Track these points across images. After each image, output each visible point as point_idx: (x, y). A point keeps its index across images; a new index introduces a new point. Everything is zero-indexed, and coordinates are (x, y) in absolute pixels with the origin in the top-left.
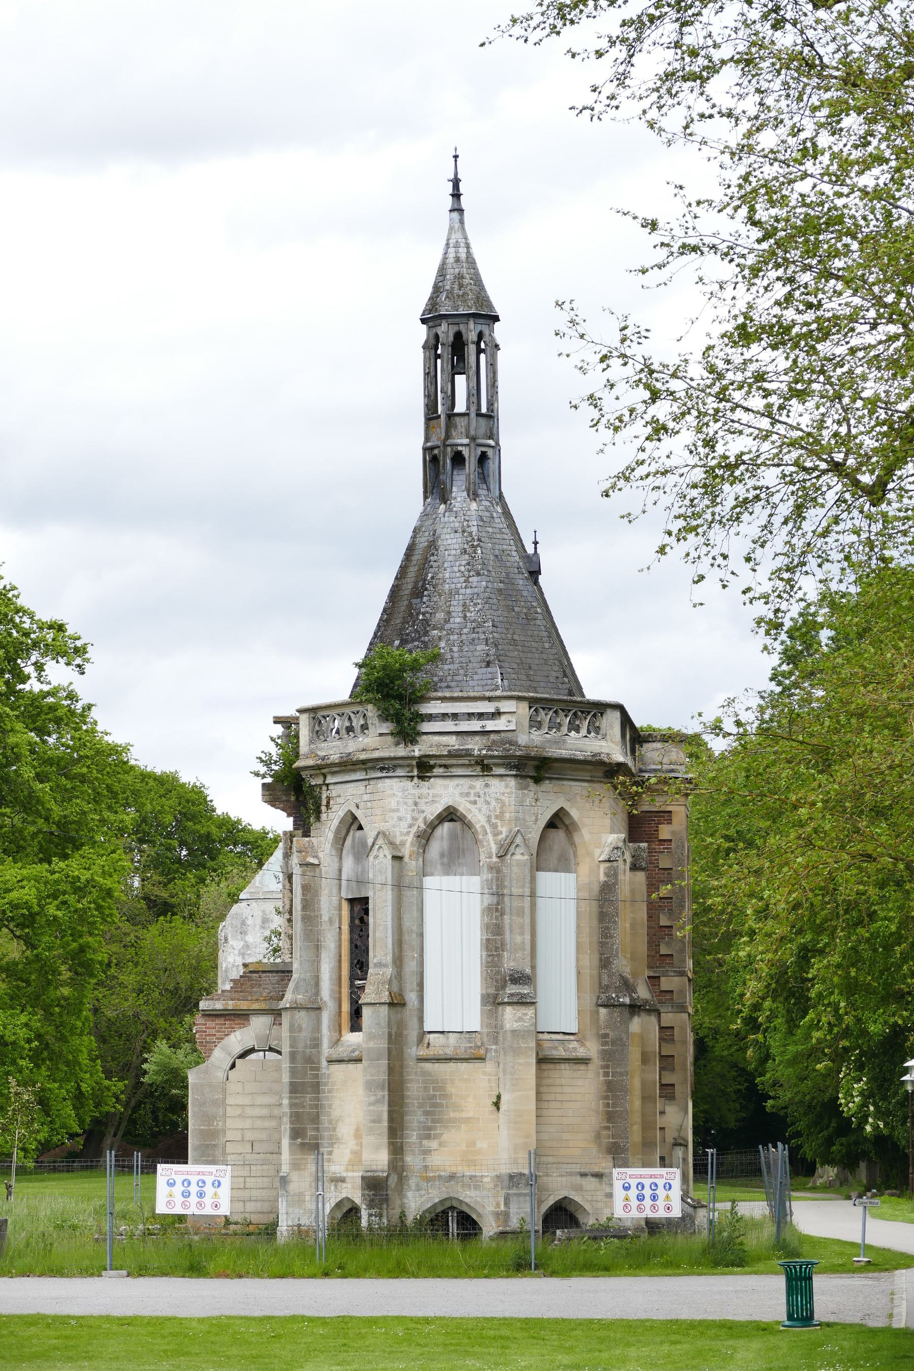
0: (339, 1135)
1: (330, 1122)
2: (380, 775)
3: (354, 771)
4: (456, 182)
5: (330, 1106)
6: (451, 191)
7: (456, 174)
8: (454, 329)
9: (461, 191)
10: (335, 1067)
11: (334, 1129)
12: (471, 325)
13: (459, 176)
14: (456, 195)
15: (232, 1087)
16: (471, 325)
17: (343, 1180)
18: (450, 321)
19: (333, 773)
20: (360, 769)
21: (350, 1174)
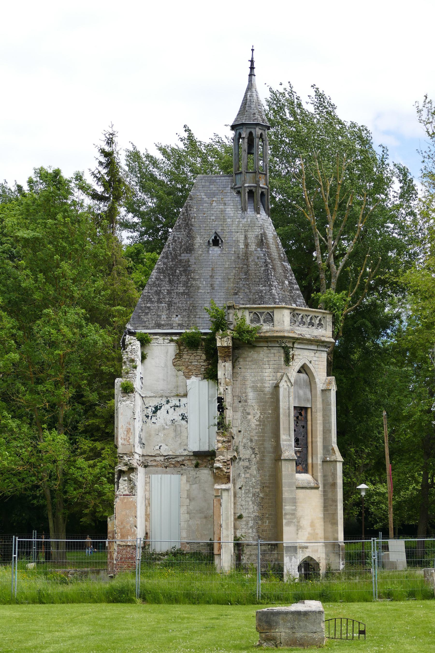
0: (302, 525)
3: (312, 344)
4: (252, 61)
6: (250, 66)
7: (252, 58)
8: (248, 130)
9: (255, 66)
12: (257, 129)
13: (254, 60)
14: (252, 68)
16: (257, 129)
17: (306, 548)
19: (299, 343)
20: (316, 345)
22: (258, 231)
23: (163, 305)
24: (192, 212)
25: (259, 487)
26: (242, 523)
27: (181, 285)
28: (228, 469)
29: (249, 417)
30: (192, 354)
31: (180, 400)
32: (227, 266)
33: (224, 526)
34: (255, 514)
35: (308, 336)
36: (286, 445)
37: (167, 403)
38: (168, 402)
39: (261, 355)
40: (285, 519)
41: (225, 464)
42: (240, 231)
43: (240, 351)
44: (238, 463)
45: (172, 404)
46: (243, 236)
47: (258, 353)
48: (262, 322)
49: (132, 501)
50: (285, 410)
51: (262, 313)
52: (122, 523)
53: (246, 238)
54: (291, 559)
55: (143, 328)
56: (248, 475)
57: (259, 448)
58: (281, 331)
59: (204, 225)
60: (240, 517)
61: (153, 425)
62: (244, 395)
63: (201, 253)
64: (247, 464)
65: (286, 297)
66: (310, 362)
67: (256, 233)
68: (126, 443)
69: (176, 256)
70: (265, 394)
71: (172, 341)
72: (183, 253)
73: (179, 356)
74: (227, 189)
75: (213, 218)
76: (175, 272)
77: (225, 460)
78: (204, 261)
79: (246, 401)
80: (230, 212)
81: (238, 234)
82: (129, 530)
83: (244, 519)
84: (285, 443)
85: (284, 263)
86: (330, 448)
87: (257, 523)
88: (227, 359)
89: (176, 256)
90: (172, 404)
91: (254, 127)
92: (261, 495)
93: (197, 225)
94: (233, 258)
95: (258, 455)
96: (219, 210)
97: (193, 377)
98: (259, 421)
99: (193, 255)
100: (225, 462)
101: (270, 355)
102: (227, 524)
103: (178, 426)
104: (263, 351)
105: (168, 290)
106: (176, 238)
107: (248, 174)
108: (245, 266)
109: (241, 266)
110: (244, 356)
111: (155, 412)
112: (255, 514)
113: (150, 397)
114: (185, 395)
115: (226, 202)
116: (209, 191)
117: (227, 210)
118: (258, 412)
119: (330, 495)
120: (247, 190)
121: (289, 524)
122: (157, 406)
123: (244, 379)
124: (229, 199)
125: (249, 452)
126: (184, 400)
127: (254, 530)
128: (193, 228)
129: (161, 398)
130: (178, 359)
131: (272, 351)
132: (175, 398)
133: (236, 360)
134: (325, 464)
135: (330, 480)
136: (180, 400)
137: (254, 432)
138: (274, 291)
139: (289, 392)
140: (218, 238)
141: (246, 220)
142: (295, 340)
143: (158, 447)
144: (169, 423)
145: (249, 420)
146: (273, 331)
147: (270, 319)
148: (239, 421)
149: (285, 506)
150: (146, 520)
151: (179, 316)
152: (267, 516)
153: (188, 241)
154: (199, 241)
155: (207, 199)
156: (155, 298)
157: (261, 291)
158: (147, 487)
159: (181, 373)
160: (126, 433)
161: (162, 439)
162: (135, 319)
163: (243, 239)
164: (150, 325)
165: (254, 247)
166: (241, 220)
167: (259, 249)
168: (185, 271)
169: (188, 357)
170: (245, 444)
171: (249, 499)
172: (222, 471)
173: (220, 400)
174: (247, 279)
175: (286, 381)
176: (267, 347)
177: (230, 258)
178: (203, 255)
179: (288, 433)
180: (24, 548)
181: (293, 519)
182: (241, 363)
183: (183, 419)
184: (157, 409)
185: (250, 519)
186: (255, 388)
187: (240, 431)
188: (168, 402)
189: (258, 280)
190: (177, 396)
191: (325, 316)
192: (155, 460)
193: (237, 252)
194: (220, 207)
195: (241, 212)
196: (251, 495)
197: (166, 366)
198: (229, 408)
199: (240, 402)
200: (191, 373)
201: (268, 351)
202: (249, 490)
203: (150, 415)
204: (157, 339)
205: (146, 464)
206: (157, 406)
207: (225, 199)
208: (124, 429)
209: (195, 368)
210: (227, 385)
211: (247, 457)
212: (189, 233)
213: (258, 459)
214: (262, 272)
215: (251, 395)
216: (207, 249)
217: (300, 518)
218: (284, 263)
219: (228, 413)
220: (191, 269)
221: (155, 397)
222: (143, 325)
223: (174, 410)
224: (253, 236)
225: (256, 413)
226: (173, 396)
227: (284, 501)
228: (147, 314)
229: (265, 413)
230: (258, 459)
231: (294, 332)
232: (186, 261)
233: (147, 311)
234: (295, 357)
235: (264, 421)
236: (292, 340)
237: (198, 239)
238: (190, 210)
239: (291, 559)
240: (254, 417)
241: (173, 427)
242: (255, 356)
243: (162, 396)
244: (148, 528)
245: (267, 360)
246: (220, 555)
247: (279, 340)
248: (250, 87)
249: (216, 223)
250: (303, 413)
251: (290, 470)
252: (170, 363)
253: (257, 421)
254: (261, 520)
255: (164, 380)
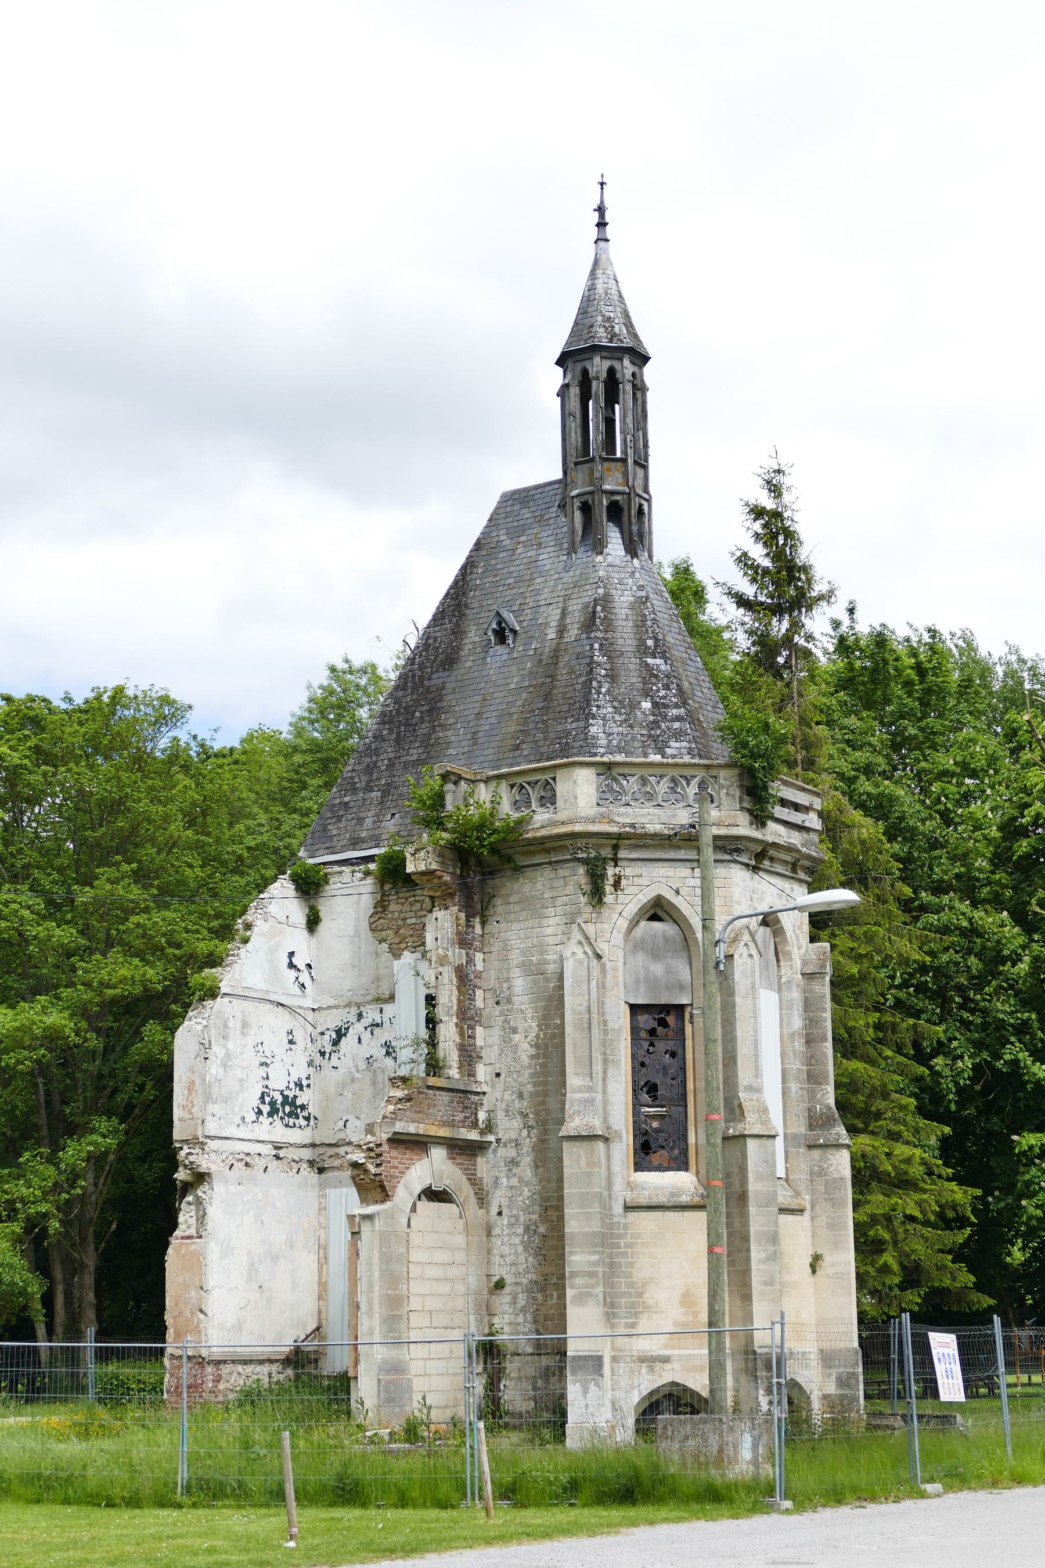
0: (650, 1302)
1: (632, 1285)
2: (727, 857)
4: (601, 210)
5: (631, 1265)
8: (607, 364)
9: (607, 220)
10: (633, 1216)
11: (640, 1295)
12: (597, 359)
14: (602, 225)
15: (415, 1239)
16: (597, 359)
17: (666, 1360)
18: (604, 354)
19: (635, 847)
21: (676, 1352)
22: (589, 594)
23: (373, 794)
25: (537, 1208)
26: (503, 1300)
27: (417, 744)
28: (378, 1165)
29: (517, 1038)
30: (406, 899)
31: (381, 1011)
32: (513, 686)
33: (363, 1307)
34: (529, 1276)
35: (651, 828)
36: (580, 1101)
37: (359, 1020)
38: (360, 1016)
39: (539, 886)
40: (572, 1287)
41: (373, 1154)
42: (556, 600)
43: (497, 880)
44: (495, 1151)
45: (366, 1021)
47: (533, 881)
48: (534, 805)
49: (194, 1250)
50: (580, 1013)
51: (533, 784)
52: (177, 1304)
54: (585, 1391)
55: (326, 851)
56: (514, 1181)
57: (536, 1113)
58: (571, 822)
60: (500, 1285)
61: (334, 1072)
62: (505, 985)
64: (512, 1153)
65: (633, 739)
66: (677, 892)
67: (587, 599)
68: (187, 1116)
69: (422, 679)
70: (547, 980)
71: (367, 873)
73: (381, 906)
74: (551, 510)
76: (413, 717)
77: (371, 1145)
79: (509, 1001)
81: (551, 607)
82: (188, 1320)
83: (508, 1289)
84: (579, 1095)
85: (650, 661)
86: (736, 1103)
87: (534, 1299)
88: (449, 902)
89: (422, 679)
90: (366, 1021)
91: (619, 355)
92: (542, 1229)
93: (475, 605)
94: (529, 665)
95: (535, 1131)
97: (406, 953)
98: (537, 1046)
100: (370, 1149)
101: (556, 884)
102: (370, 1303)
103: (378, 1072)
104: (542, 876)
105: (389, 759)
106: (431, 641)
108: (549, 680)
110: (504, 891)
111: (336, 1043)
112: (529, 1276)
113: (329, 1008)
114: (392, 998)
116: (515, 524)
118: (534, 1025)
119: (737, 1223)
120: (577, 504)
121: (582, 1298)
122: (340, 1029)
123: (506, 949)
125: (517, 1123)
126: (389, 1009)
127: (529, 1318)
128: (467, 612)
129: (347, 1010)
130: (379, 915)
131: (561, 873)
132: (373, 1007)
133: (489, 902)
134: (727, 1142)
135: (737, 1187)
136: (381, 1011)
137: (526, 1074)
138: (593, 730)
139: (589, 968)
142: (617, 841)
143: (341, 1124)
144: (363, 1065)
145: (517, 1046)
146: (554, 824)
147: (549, 799)
148: (496, 1050)
149: (572, 1253)
150: (320, 1298)
151: (397, 815)
152: (555, 1280)
154: (473, 640)
155: (508, 542)
156: (361, 783)
157: (568, 733)
158: (322, 1219)
159: (385, 946)
160: (186, 1092)
161: (350, 1103)
162: (316, 835)
163: (558, 617)
164: (341, 844)
168: (430, 711)
169: (398, 907)
170: (508, 1105)
171: (517, 1240)
172: (366, 1171)
173: (430, 1000)
174: (545, 709)
175: (580, 943)
176: (550, 863)
179: (587, 1071)
180: (23, 1366)
181: (593, 1286)
182: (500, 909)
183: (388, 1054)
184: (341, 1033)
185: (520, 1290)
186: (526, 967)
187: (498, 1075)
188: (360, 1016)
189: (565, 708)
190: (378, 1000)
191: (714, 772)
192: (337, 1155)
196: (520, 1230)
197: (357, 933)
198: (444, 1019)
199: (498, 1003)
200: (404, 945)
201: (552, 875)
202: (517, 1217)
203: (328, 1051)
204: (341, 872)
205: (320, 1165)
206: (340, 1029)
208: (183, 1084)
209: (411, 932)
210: (442, 965)
211: (513, 1137)
212: (457, 625)
213: (534, 1139)
215: (520, 984)
217: (644, 1285)
218: (650, 661)
219: (442, 1033)
220: (444, 704)
221: (337, 1007)
222: (327, 845)
223: (372, 1034)
225: (530, 1027)
226: (369, 1003)
227: (567, 1241)
228: (339, 818)
229: (547, 1026)
230: (534, 1139)
231: (611, 821)
233: (341, 813)
234: (623, 882)
235: (546, 1045)
236: (609, 841)
237: (472, 634)
239: (585, 1391)
240: (526, 1037)
241: (370, 1075)
242: (527, 889)
243: (348, 1005)
244: (323, 1316)
245: (550, 895)
246: (356, 1378)
247: (568, 843)
249: (514, 591)
250: (671, 1020)
251: (583, 1162)
252: (365, 924)
253: (531, 1046)
254: (542, 1290)
255: (353, 966)
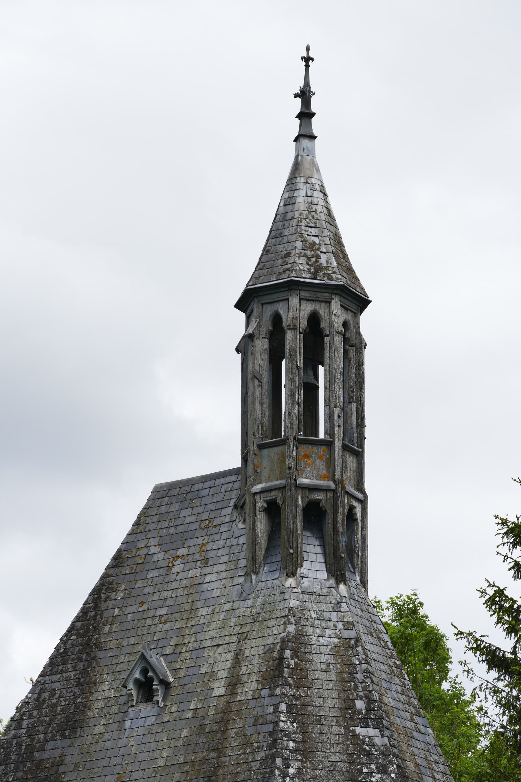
4: (305, 95)
7: (307, 83)
8: (308, 308)
9: (313, 109)
24: (110, 604)
42: (227, 639)
46: (230, 656)
53: (238, 659)
59: (132, 641)
63: (101, 729)
67: (271, 640)
69: (31, 749)
72: (53, 739)
74: (224, 512)
75: (163, 611)
78: (101, 755)
80: (213, 585)
81: (219, 650)
85: (359, 730)
89: (31, 749)
91: (326, 296)
96: (185, 582)
99: (78, 742)
106: (46, 695)
107: (265, 451)
108: (213, 755)
109: (200, 756)
115: (211, 554)
116: (172, 530)
117: (208, 579)
120: (261, 503)
124: (221, 543)
140: (150, 674)
141: (250, 602)
153: (76, 698)
154: (106, 694)
163: (229, 665)
165: (254, 686)
166: (236, 604)
167: (265, 692)
177: (177, 734)
178: (106, 736)
193: (200, 713)
194: (191, 574)
195: (241, 580)
207: (209, 547)
212: (84, 673)
214: (255, 766)
216: (119, 717)
218: (359, 730)
224: (260, 651)
232: (53, 765)
238: (107, 599)
248: (300, 171)
249: (166, 627)
